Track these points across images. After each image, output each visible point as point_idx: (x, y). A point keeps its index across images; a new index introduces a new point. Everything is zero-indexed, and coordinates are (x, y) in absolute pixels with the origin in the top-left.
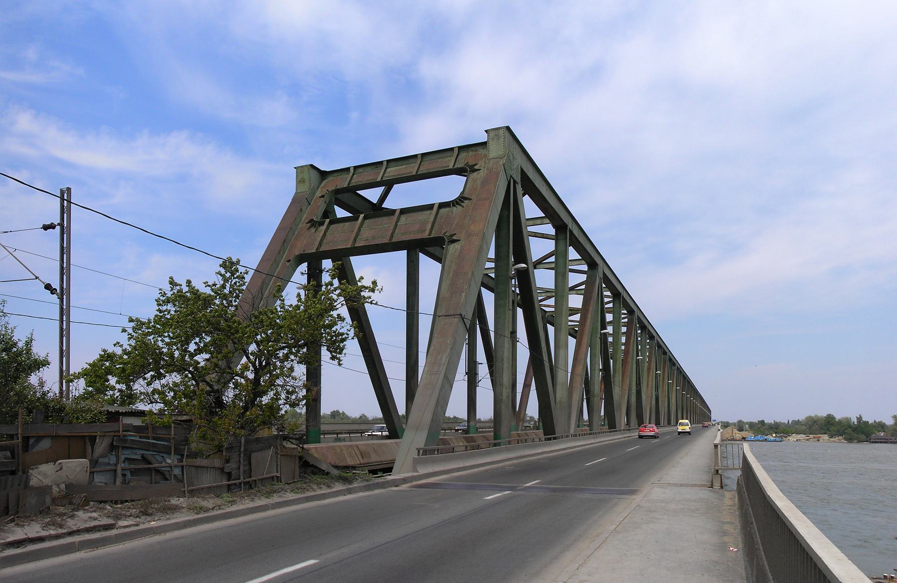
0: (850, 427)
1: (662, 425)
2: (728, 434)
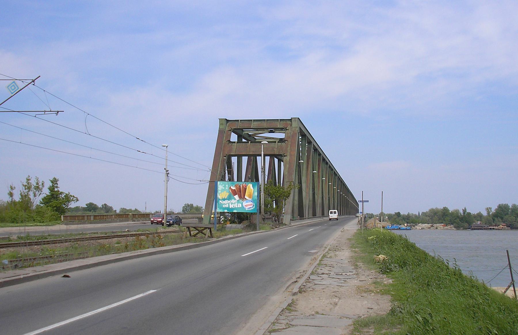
0: (458, 217)
1: (318, 216)
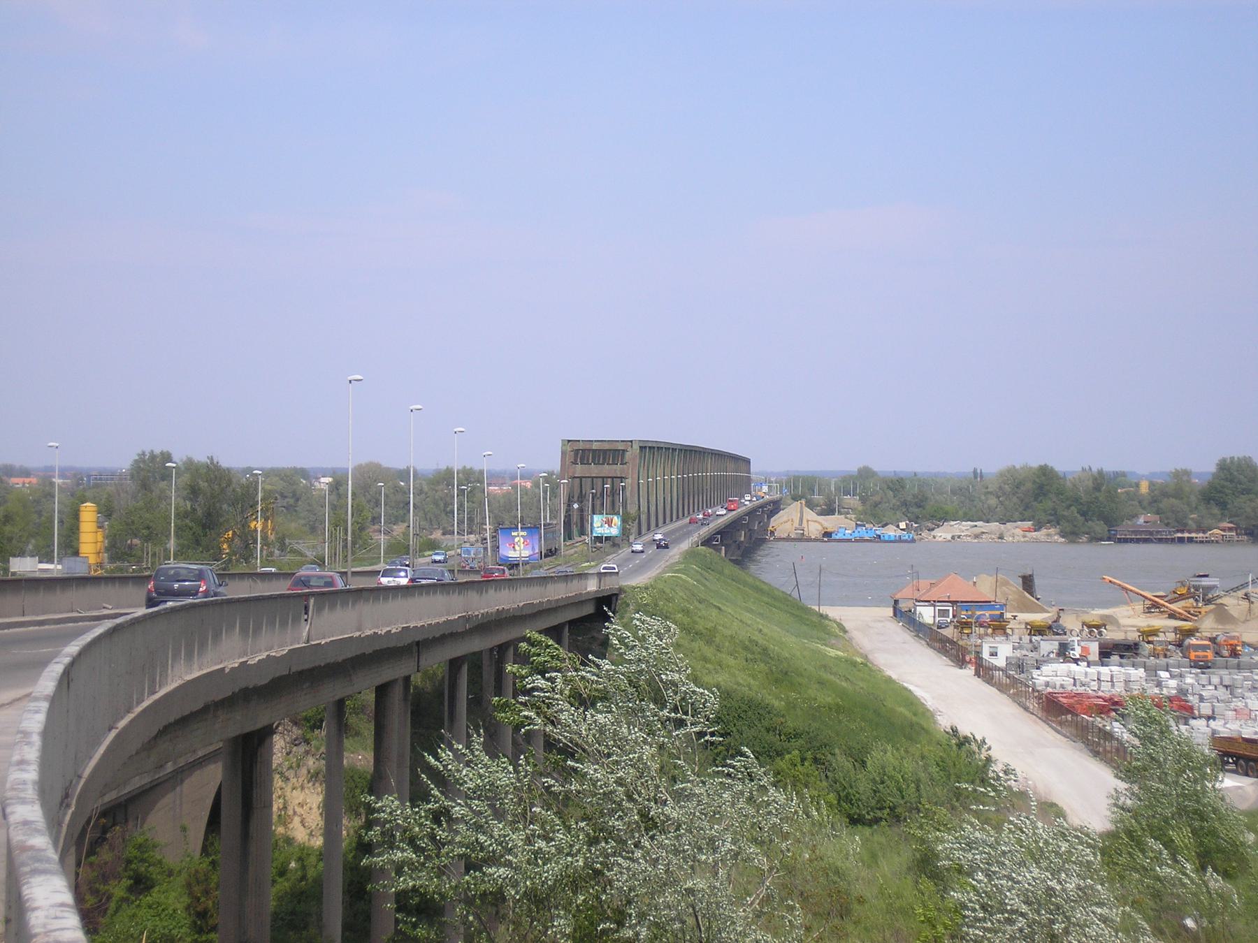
2: (790, 523)
